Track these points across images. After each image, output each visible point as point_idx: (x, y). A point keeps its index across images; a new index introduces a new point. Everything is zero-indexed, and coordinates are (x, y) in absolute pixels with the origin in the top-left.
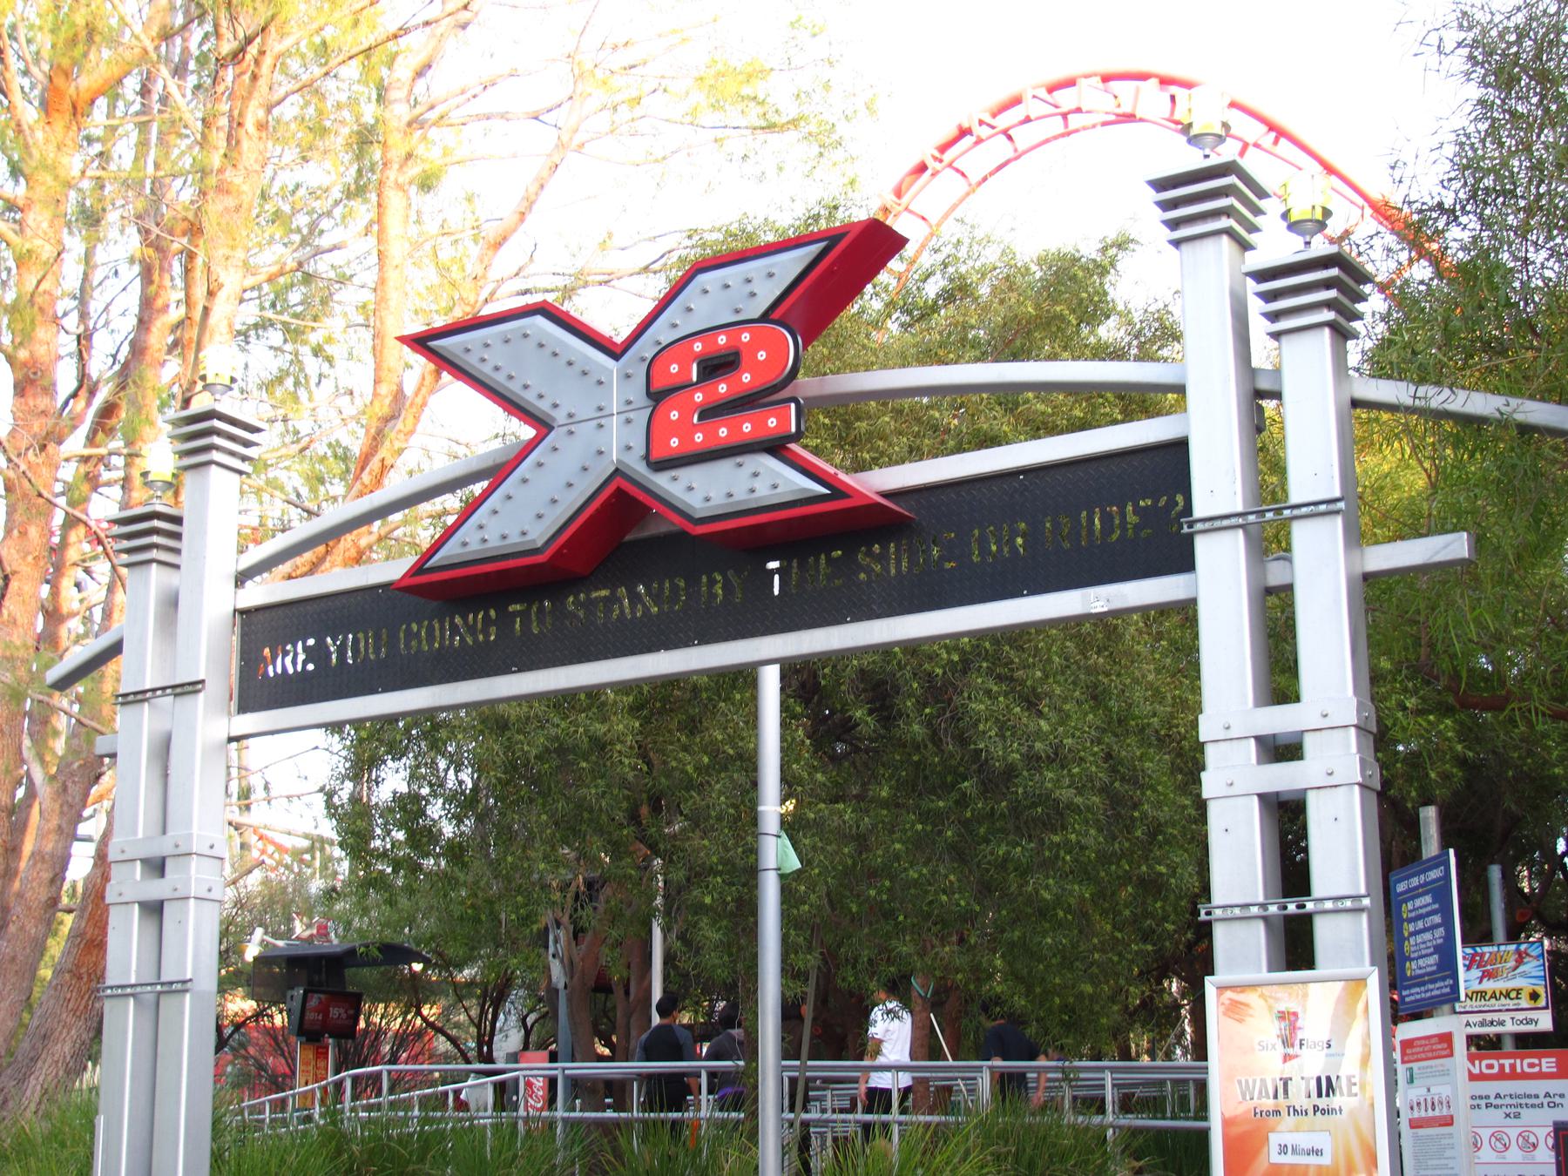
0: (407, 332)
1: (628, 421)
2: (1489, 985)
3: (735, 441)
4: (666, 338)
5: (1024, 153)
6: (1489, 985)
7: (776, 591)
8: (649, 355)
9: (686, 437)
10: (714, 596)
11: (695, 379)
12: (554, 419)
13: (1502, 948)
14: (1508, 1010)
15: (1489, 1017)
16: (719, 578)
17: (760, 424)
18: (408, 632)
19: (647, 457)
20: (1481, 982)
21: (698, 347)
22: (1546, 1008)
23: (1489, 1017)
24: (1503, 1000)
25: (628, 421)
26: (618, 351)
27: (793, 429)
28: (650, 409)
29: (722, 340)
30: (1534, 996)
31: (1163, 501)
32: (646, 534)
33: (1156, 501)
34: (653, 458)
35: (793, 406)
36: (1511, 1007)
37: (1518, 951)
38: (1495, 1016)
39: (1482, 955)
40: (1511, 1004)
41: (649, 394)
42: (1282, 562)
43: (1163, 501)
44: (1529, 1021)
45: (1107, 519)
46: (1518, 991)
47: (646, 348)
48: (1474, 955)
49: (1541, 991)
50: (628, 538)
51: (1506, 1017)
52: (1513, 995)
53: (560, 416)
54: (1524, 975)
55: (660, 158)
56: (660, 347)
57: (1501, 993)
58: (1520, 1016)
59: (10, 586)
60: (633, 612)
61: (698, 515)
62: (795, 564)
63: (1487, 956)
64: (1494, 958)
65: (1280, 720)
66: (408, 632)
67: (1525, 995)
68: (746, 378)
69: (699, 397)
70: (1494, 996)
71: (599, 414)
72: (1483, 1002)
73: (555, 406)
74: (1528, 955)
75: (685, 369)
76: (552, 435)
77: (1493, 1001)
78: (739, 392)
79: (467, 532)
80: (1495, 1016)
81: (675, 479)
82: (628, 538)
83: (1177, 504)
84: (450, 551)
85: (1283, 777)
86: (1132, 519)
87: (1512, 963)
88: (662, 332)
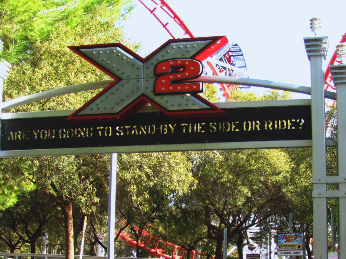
1: (148, 81)
2: (287, 243)
4: (161, 59)
5: (154, 15)
6: (287, 243)
7: (184, 132)
8: (155, 63)
10: (164, 131)
13: (292, 234)
14: (292, 250)
15: (287, 251)
16: (166, 126)
18: (62, 131)
20: (285, 243)
22: (302, 250)
23: (287, 251)
24: (291, 248)
25: (148, 81)
30: (299, 247)
31: (298, 121)
32: (145, 111)
33: (296, 120)
36: (293, 249)
37: (296, 235)
38: (289, 251)
39: (287, 236)
40: (293, 248)
42: (332, 141)
43: (298, 121)
44: (297, 253)
45: (282, 124)
46: (295, 245)
47: (154, 61)
48: (284, 236)
49: (301, 245)
51: (291, 252)
52: (294, 246)
53: (125, 76)
54: (297, 241)
56: (158, 62)
57: (291, 246)
58: (295, 251)
60: (139, 133)
62: (190, 124)
63: (288, 236)
64: (290, 237)
65: (332, 179)
66: (62, 131)
67: (297, 246)
70: (289, 246)
72: (286, 248)
73: (123, 73)
74: (298, 236)
75: (167, 69)
77: (288, 248)
79: (93, 105)
80: (289, 251)
81: (162, 99)
83: (302, 122)
84: (87, 111)
85: (334, 193)
86: (290, 124)
87: (294, 238)
88: (160, 57)
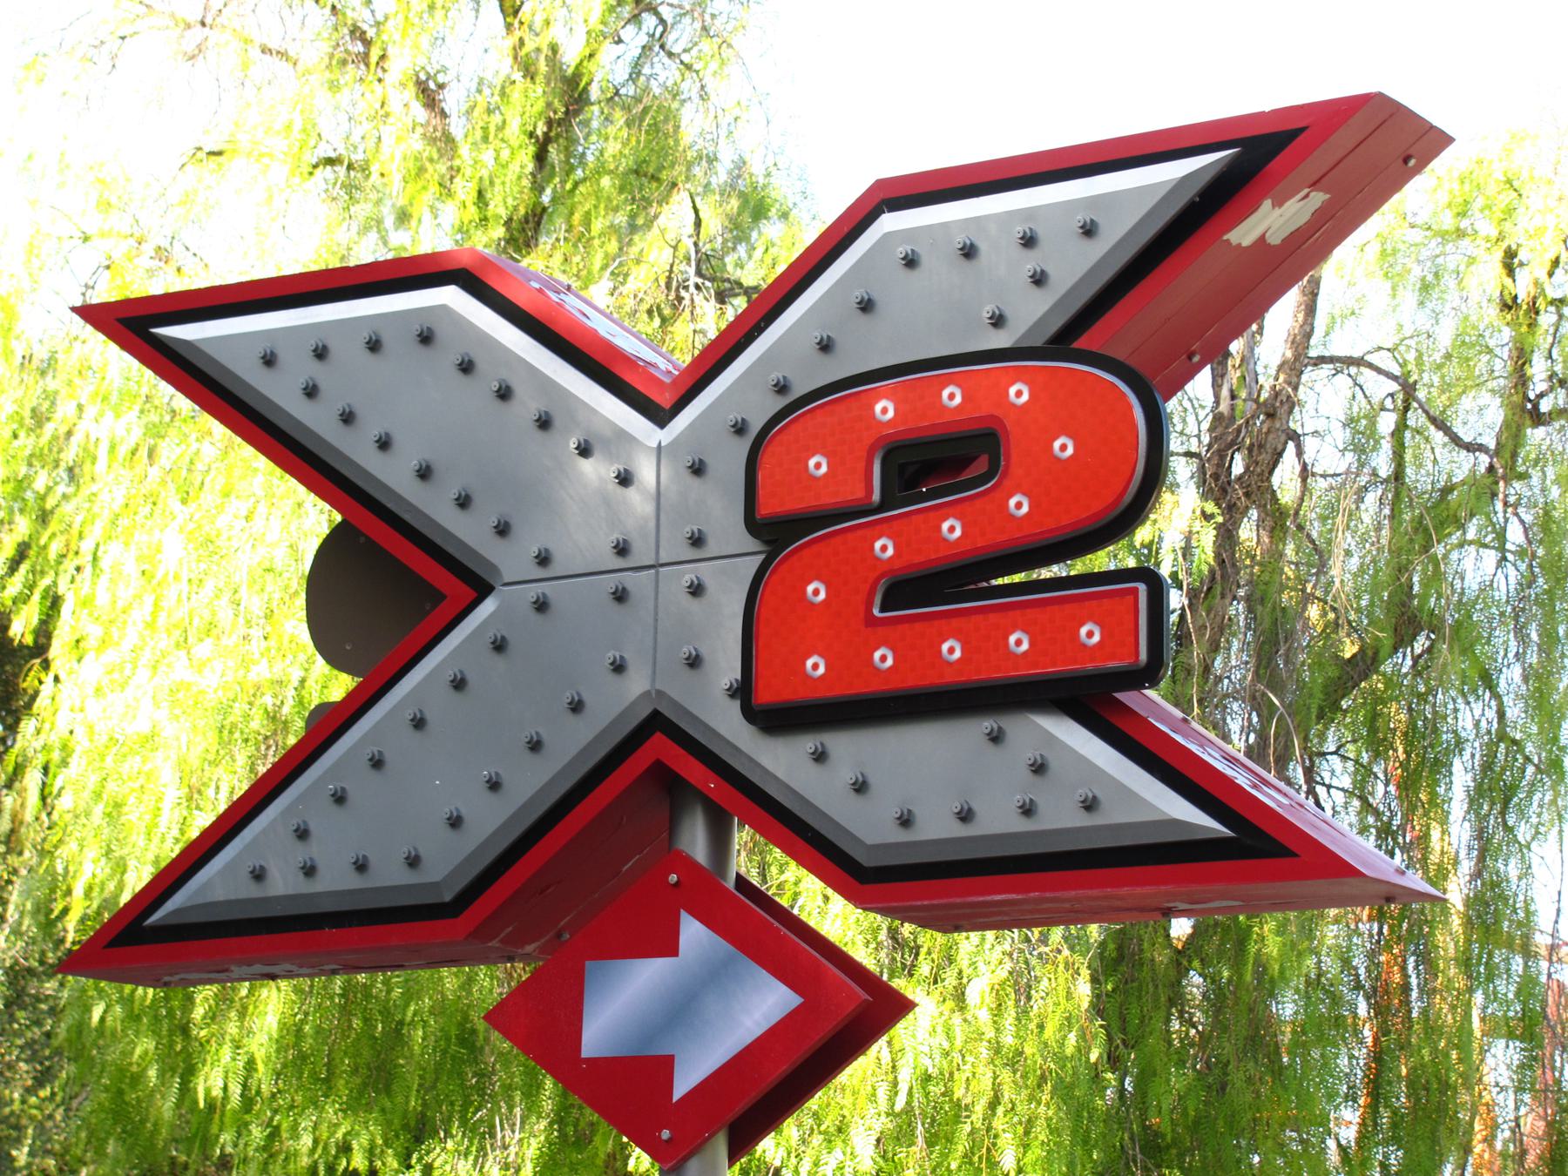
0: (96, 298)
3: (914, 680)
4: (812, 375)
9: (848, 658)
11: (876, 496)
12: (494, 568)
17: (983, 645)
19: (743, 691)
21: (885, 410)
26: (665, 400)
27: (1143, 656)
28: (762, 557)
29: (952, 396)
34: (765, 696)
35: (1142, 588)
41: (754, 525)
50: (1224, 831)
55: (116, 61)
59: (1464, 453)
61: (866, 861)
68: (1019, 504)
69: (884, 547)
71: (620, 563)
76: (488, 607)
78: (924, 557)
82: (1224, 831)
